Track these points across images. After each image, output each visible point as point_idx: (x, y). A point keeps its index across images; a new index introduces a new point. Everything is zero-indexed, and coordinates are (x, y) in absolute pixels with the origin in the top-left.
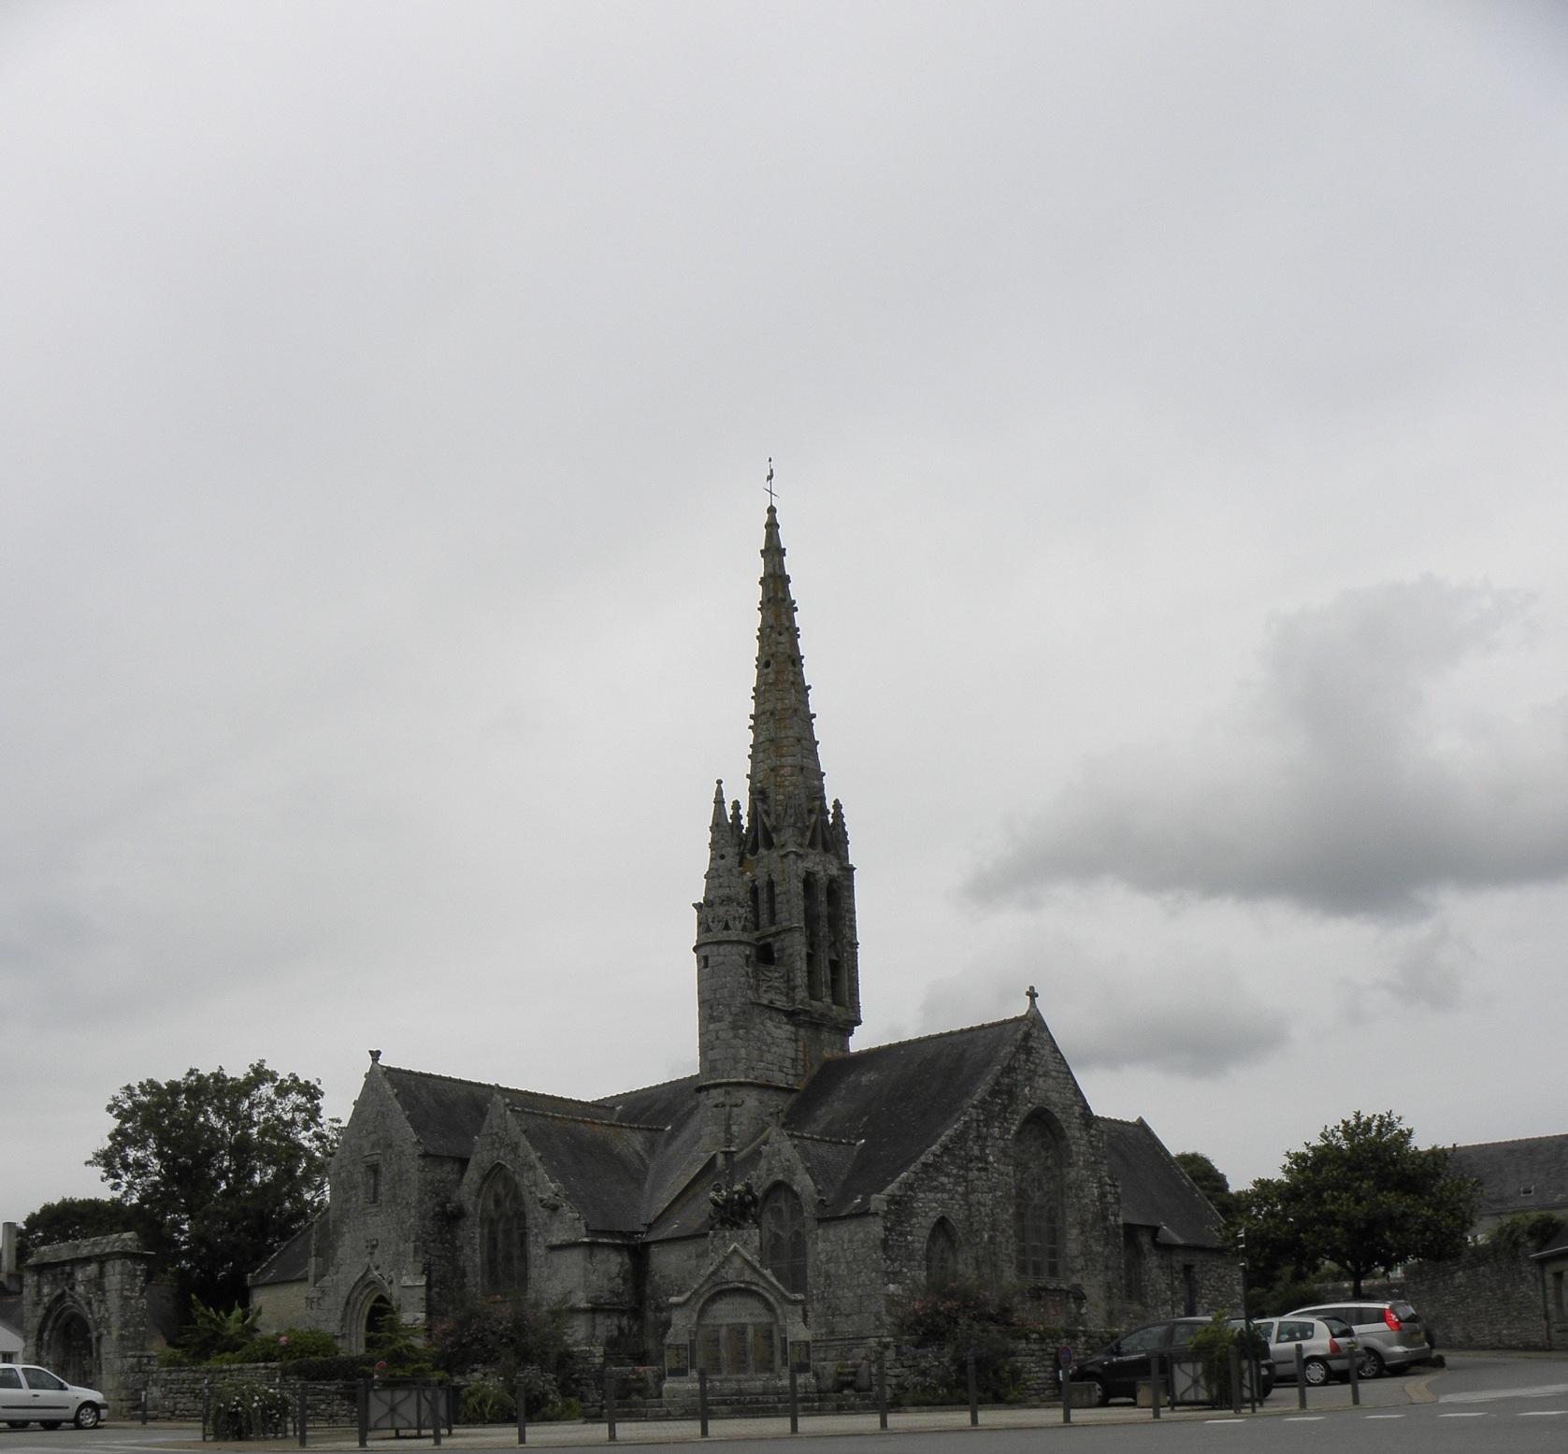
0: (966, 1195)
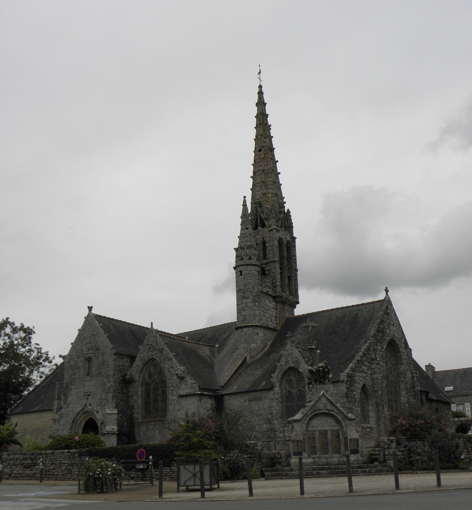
0: (371, 374)
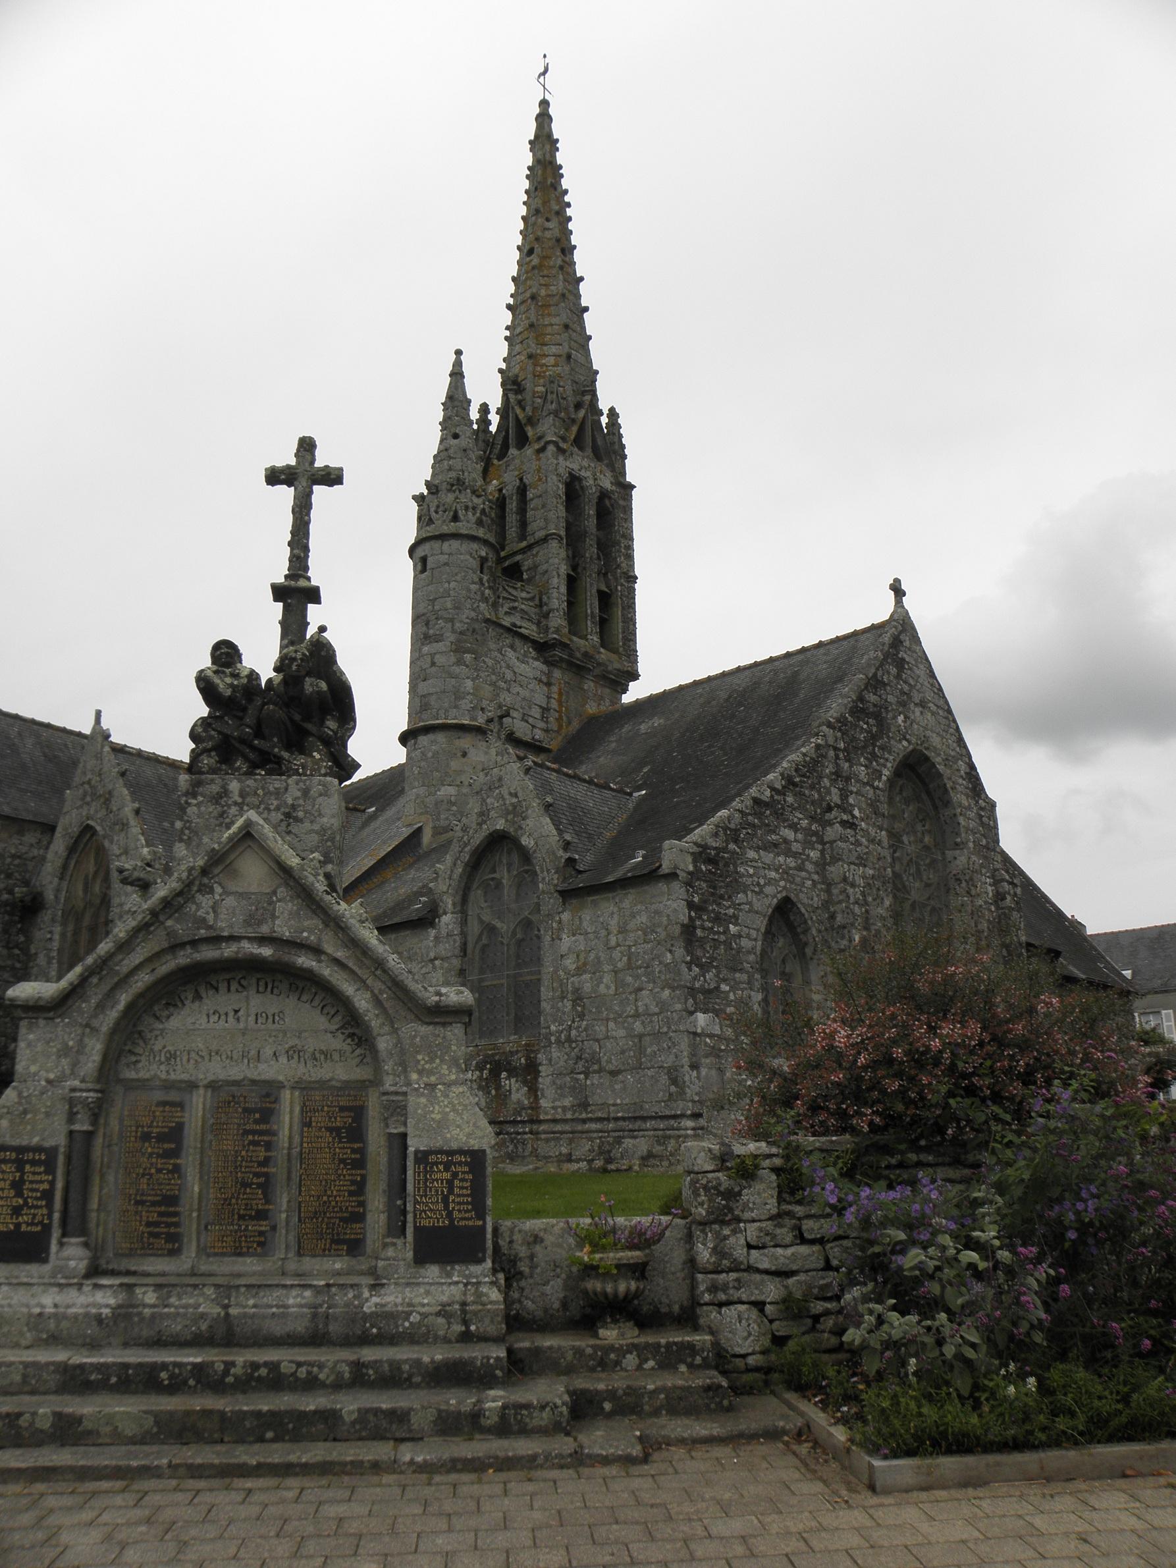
0: (822, 865)
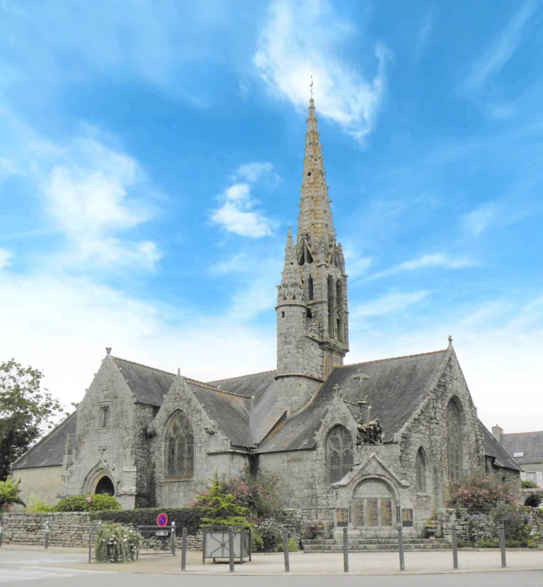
0: (430, 436)
